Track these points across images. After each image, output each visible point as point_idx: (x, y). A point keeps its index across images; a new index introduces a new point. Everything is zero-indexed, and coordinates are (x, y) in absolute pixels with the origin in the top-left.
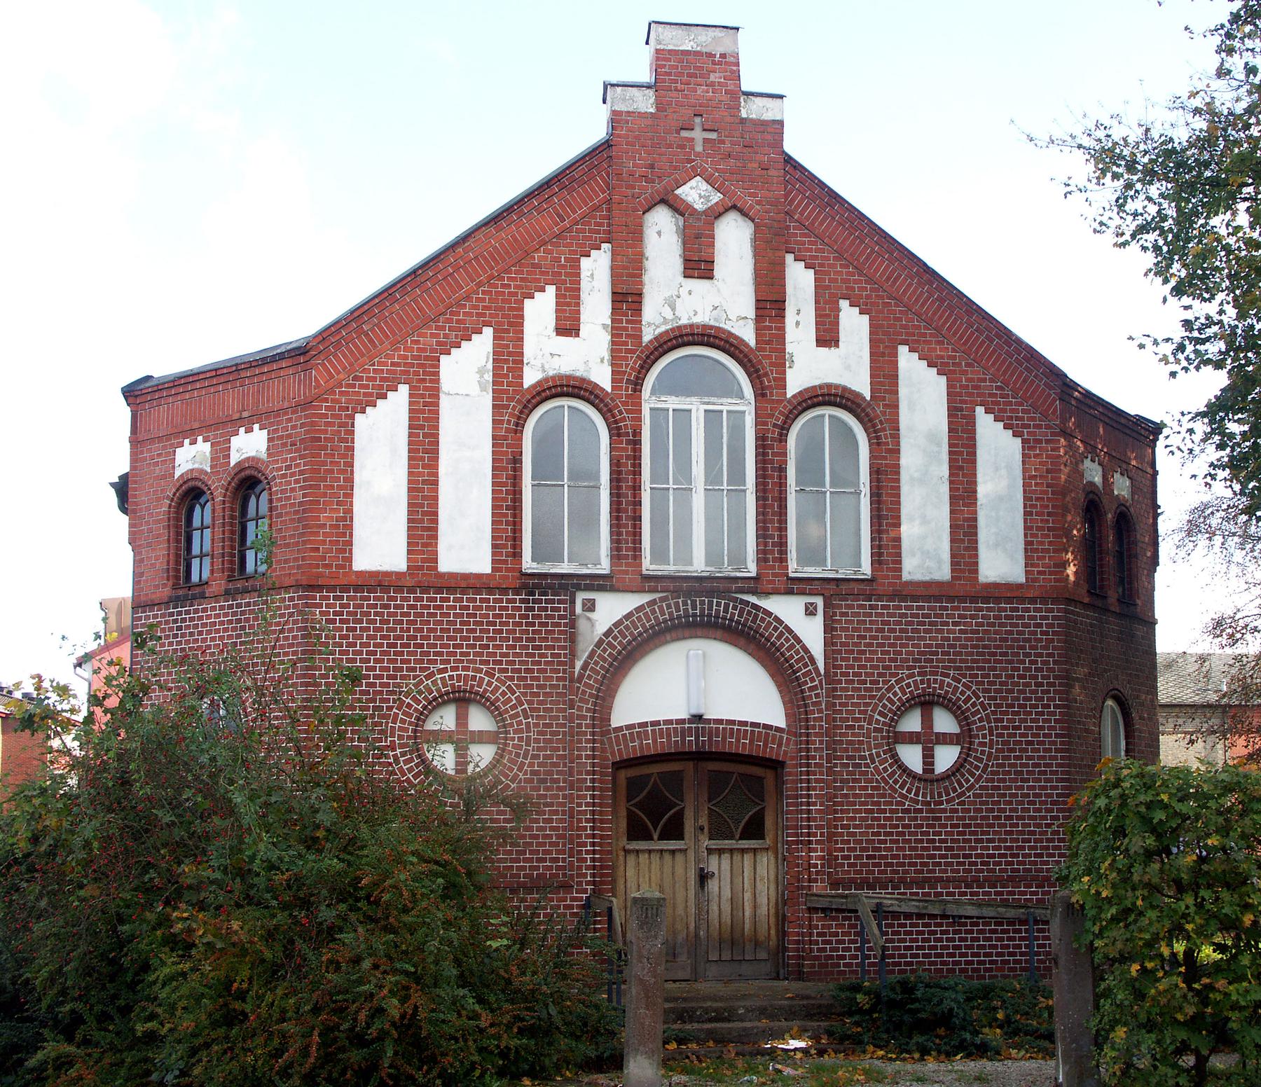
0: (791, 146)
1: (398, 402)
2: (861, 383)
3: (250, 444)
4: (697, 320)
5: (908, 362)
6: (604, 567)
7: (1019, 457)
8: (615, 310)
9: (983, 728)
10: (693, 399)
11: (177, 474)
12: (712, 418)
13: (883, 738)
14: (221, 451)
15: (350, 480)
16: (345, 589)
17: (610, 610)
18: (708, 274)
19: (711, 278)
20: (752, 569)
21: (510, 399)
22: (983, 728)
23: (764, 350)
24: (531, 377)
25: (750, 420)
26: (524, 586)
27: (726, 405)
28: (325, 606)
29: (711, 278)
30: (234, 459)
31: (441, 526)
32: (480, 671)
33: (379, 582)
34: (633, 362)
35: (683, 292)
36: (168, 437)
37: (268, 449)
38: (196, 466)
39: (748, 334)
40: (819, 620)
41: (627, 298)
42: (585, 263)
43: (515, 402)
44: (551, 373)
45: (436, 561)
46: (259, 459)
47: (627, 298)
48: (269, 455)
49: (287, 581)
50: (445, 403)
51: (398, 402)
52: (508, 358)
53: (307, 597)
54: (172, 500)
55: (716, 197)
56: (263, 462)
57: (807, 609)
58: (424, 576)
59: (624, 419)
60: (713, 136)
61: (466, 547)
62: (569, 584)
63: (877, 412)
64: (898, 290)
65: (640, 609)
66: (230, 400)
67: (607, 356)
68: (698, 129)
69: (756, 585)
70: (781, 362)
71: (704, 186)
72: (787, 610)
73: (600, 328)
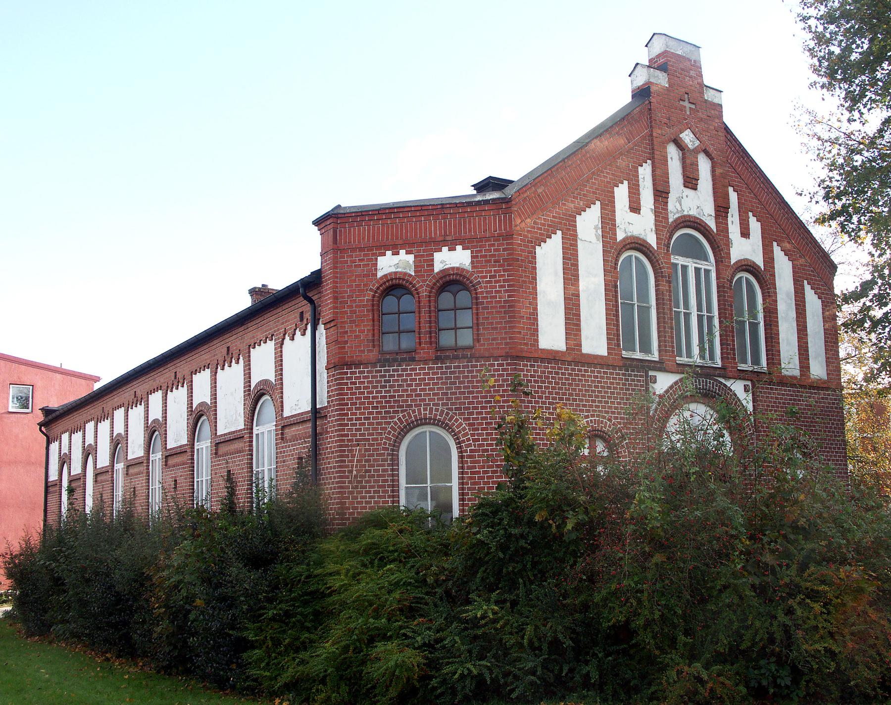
0: (728, 119)
1: (556, 241)
2: (759, 261)
3: (453, 258)
4: (691, 213)
5: (778, 253)
6: (655, 356)
7: (821, 310)
8: (656, 201)
9: (431, 409)
10: (690, 260)
11: (380, 274)
12: (697, 270)
13: (436, 415)
14: (424, 263)
15: (535, 288)
16: (536, 360)
17: (663, 382)
18: (695, 188)
19: (696, 189)
20: (719, 363)
21: (612, 248)
22: (431, 409)
23: (720, 235)
24: (620, 236)
25: (713, 275)
26: (625, 366)
27: (703, 265)
28: (527, 371)
29: (696, 189)
30: (437, 268)
31: (582, 324)
32: (604, 417)
33: (552, 357)
34: (665, 233)
35: (684, 195)
36: (370, 249)
37: (472, 262)
38: (399, 270)
39: (712, 224)
40: (750, 397)
41: (661, 193)
42: (640, 169)
43: (615, 248)
44: (629, 234)
45: (580, 345)
46: (463, 270)
47: (661, 193)
48: (473, 267)
49: (496, 353)
50: (580, 245)
51: (556, 241)
52: (608, 222)
53: (516, 364)
54: (376, 292)
55: (697, 143)
56: (468, 271)
57: (745, 389)
58: (573, 356)
59: (663, 267)
60: (693, 106)
61: (595, 341)
62: (645, 366)
63: (764, 277)
64: (378, 240)
65: (676, 383)
66: (434, 228)
67: (654, 229)
68: (687, 102)
69: (724, 372)
70: (728, 243)
71: (692, 135)
72: (738, 387)
73: (649, 211)
